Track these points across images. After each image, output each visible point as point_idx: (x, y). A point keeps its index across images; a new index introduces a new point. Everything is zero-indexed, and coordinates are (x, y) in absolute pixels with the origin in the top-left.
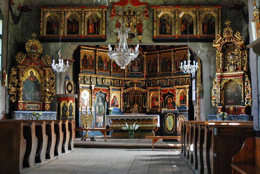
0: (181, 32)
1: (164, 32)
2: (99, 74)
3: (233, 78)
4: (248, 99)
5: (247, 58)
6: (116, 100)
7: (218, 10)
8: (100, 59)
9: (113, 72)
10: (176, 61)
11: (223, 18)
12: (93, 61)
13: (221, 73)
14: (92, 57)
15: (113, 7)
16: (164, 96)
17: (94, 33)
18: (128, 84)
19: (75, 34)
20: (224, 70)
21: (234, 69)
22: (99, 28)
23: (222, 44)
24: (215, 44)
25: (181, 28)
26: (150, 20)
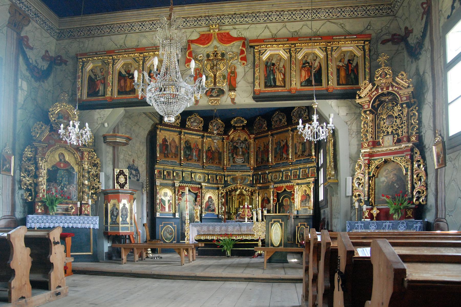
0: (301, 84)
1: (273, 84)
2: (186, 167)
3: (391, 157)
4: (419, 192)
5: (417, 120)
6: (211, 202)
7: (364, 43)
8: (188, 144)
9: (206, 163)
10: (295, 145)
11: (371, 56)
12: (177, 147)
13: (371, 149)
14: (175, 141)
15: (189, 48)
16: (278, 195)
18: (229, 180)
19: (130, 94)
20: (376, 144)
21: (393, 141)
23: (372, 98)
24: (360, 98)
25: (301, 76)
26: (249, 65)
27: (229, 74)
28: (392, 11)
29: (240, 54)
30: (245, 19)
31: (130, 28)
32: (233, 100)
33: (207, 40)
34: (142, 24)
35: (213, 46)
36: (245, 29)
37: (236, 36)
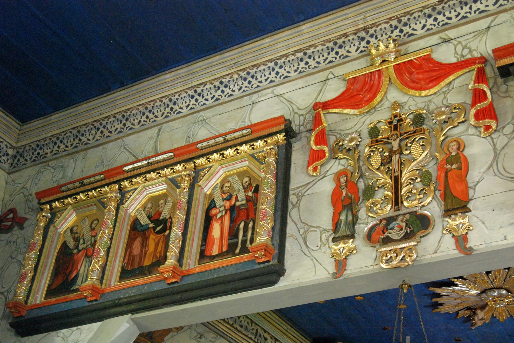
15: (317, 120)
17: (231, 250)
22: (251, 225)
27: (440, 168)
29: (474, 104)
31: (168, 110)
32: (461, 241)
33: (369, 90)
34: (197, 93)
35: (387, 104)
36: (478, 33)
37: (454, 60)
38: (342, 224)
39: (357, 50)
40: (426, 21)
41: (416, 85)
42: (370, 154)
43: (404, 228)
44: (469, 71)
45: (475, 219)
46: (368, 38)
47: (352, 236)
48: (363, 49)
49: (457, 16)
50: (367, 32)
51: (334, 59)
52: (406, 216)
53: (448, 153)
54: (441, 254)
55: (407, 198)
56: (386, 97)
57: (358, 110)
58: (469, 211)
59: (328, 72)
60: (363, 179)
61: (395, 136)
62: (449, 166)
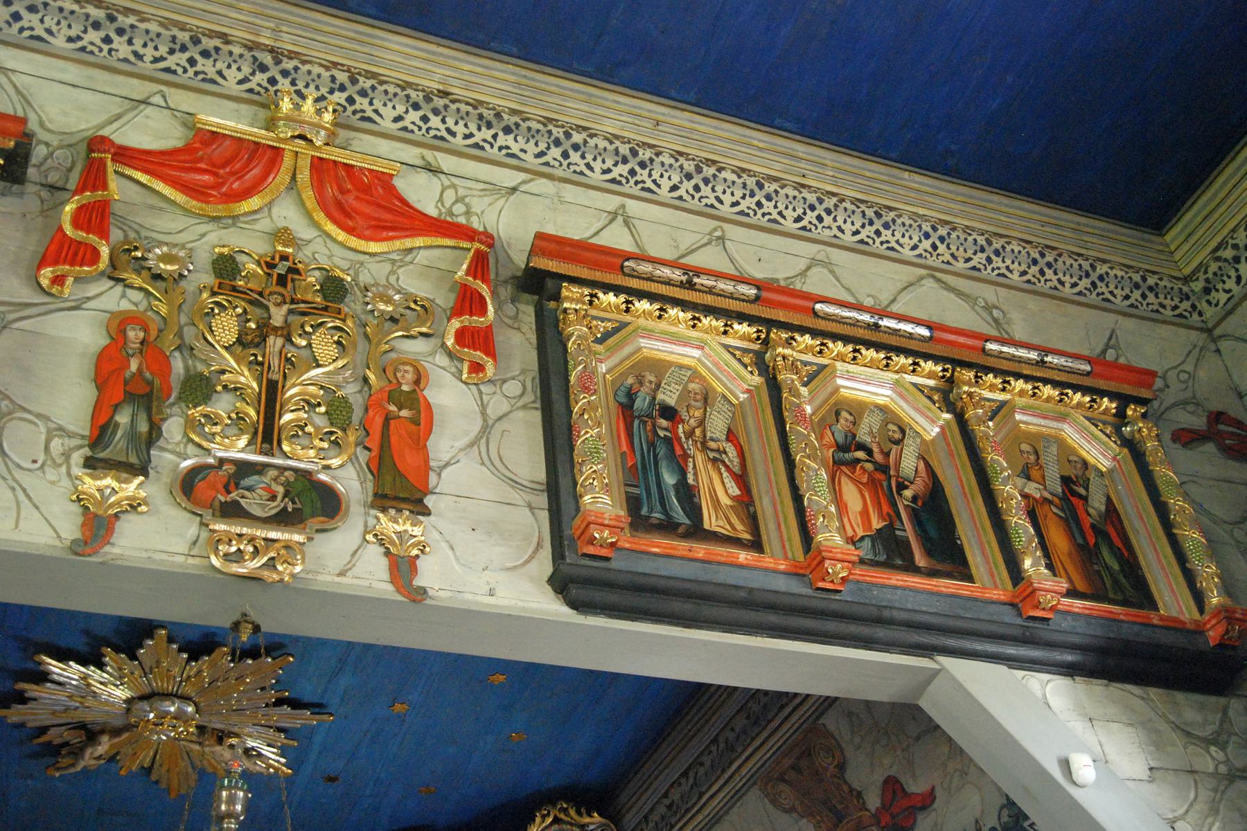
15: (94, 177)
28: (1194, 307)
30: (503, 139)
32: (403, 568)
35: (264, 224)
36: (492, 189)
37: (432, 212)
38: (119, 434)
39: (240, 82)
40: (407, 112)
41: (341, 214)
42: (212, 309)
43: (279, 498)
44: (455, 248)
45: (436, 535)
46: (274, 72)
47: (142, 469)
48: (258, 89)
49: (467, 137)
50: (278, 62)
51: (180, 71)
52: (286, 473)
53: (394, 381)
54: (355, 581)
55: (293, 436)
56: (270, 210)
57: (199, 205)
58: (427, 512)
59: (156, 87)
60: (181, 352)
61: (279, 299)
62: (393, 408)
